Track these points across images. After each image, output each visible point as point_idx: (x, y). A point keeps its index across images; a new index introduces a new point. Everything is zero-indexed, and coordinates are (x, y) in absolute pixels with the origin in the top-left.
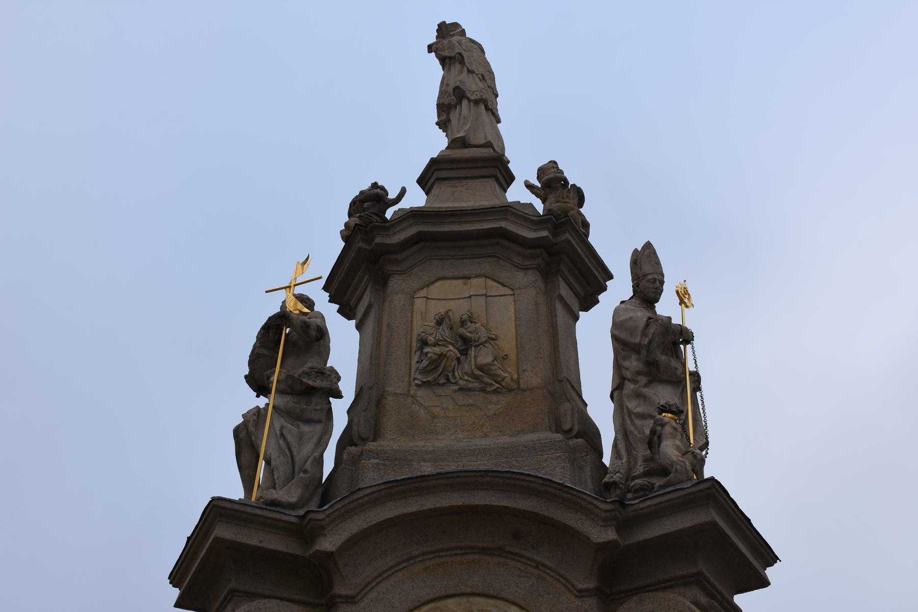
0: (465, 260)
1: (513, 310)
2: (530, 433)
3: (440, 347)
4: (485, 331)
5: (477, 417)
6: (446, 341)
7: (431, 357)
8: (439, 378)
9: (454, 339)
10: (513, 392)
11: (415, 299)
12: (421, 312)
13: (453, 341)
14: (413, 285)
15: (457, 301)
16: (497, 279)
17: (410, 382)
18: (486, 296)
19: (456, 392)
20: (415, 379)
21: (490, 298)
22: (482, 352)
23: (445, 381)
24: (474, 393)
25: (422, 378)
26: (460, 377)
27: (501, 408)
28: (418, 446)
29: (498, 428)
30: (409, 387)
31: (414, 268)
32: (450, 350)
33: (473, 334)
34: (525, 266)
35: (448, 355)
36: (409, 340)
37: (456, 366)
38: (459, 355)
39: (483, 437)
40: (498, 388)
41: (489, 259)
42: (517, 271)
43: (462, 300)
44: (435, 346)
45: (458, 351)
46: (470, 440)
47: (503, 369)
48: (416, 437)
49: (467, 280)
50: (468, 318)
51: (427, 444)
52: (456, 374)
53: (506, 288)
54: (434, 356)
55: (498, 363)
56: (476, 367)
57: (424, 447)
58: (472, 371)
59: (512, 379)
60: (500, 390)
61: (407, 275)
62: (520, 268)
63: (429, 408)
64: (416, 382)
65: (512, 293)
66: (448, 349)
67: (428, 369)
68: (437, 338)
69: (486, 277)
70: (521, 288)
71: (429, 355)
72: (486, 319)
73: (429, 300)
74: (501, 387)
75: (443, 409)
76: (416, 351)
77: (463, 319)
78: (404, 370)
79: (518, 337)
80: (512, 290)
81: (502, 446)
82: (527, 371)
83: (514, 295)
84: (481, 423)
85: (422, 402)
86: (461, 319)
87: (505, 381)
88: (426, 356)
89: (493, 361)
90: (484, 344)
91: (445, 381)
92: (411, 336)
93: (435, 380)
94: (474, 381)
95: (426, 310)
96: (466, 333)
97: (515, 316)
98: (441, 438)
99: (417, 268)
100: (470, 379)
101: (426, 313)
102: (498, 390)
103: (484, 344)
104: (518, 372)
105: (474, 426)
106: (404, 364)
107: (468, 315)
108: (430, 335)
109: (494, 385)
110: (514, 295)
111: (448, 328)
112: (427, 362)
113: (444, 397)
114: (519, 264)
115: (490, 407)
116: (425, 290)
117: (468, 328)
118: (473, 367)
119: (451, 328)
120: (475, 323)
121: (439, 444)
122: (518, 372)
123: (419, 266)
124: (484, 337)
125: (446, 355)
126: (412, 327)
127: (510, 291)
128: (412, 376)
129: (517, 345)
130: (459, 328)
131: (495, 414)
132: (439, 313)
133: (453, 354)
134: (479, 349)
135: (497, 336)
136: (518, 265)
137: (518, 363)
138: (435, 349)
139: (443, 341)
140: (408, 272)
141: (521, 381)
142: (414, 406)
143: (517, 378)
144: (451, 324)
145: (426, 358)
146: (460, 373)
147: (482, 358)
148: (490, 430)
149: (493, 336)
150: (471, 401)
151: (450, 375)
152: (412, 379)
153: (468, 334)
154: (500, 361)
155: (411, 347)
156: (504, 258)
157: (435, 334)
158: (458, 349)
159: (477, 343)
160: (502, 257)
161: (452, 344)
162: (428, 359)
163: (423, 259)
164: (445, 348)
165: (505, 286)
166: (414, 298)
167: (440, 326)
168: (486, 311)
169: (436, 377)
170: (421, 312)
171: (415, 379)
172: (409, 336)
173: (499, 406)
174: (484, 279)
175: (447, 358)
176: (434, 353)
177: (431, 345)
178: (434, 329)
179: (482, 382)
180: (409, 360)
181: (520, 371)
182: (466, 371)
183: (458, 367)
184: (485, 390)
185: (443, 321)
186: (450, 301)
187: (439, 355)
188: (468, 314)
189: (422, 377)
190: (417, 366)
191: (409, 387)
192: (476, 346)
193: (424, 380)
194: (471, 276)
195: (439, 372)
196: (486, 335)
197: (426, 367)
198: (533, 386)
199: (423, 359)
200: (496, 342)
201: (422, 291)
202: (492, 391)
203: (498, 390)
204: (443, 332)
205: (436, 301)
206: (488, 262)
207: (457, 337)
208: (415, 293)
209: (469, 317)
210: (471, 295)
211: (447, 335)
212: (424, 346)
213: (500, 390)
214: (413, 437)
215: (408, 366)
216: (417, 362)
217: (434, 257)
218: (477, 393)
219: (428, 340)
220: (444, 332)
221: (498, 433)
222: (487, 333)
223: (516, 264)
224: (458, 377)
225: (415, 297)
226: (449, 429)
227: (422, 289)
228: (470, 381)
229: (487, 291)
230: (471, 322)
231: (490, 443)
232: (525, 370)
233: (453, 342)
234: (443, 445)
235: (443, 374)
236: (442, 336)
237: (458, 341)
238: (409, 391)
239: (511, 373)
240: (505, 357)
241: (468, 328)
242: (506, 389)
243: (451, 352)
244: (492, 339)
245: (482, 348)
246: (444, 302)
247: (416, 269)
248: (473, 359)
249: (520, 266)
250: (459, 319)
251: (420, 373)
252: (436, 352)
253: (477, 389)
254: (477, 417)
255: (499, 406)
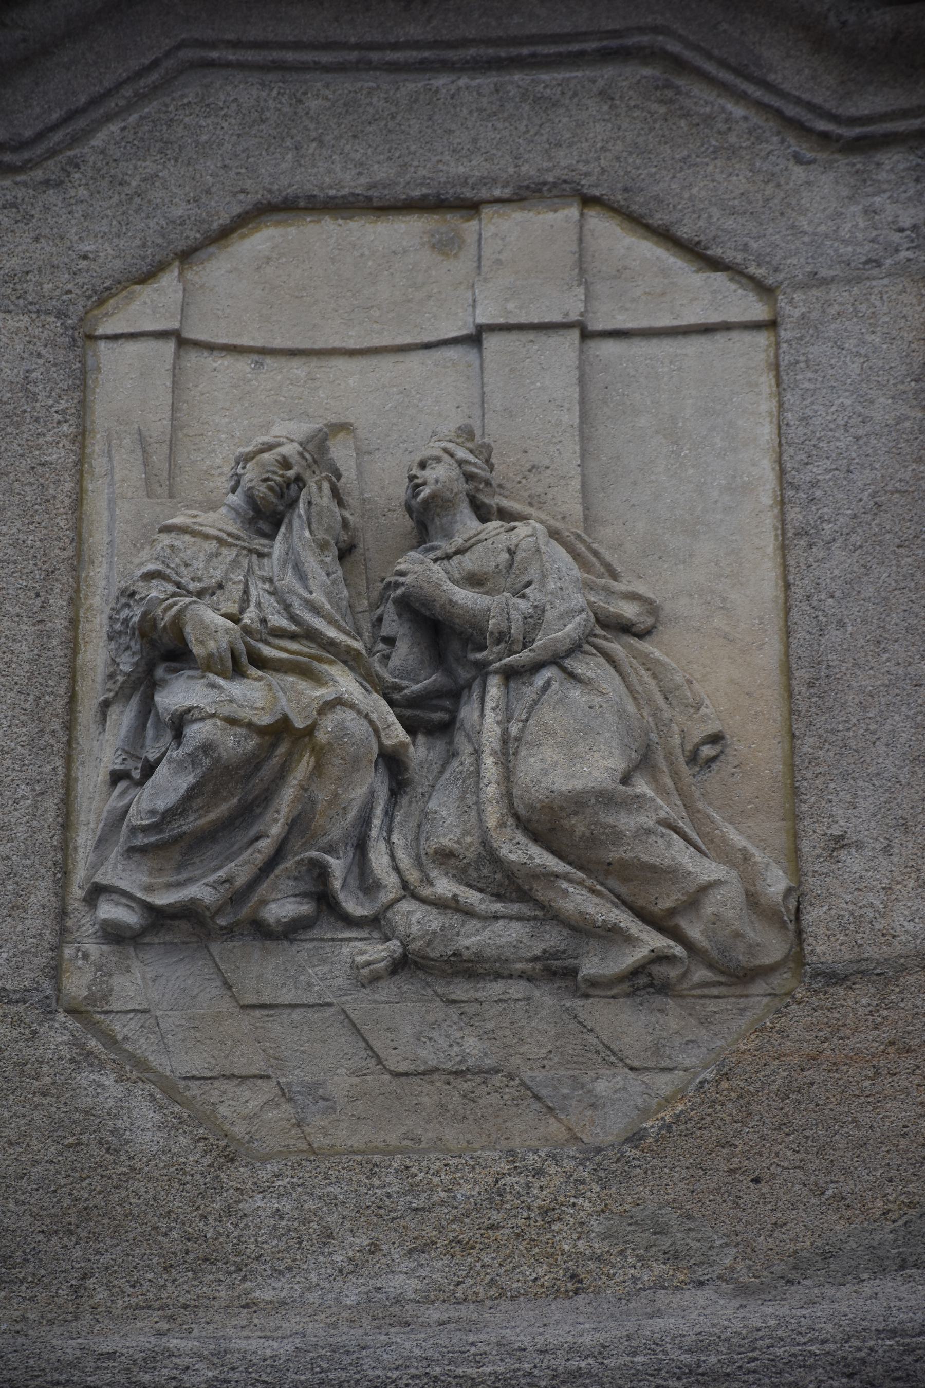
0: (441, 81)
1: (766, 432)
2: (880, 1270)
3: (273, 678)
4: (576, 572)
5: (512, 1154)
6: (310, 635)
7: (207, 748)
8: (263, 889)
9: (366, 626)
10: (760, 987)
11: (102, 345)
12: (142, 440)
13: (358, 633)
14: (86, 247)
15: (386, 366)
16: (658, 219)
17: (63, 913)
18: (586, 335)
19: (375, 979)
20: (97, 892)
21: (608, 349)
22: (548, 714)
23: (306, 908)
24: (497, 987)
25: (149, 889)
26: (405, 885)
27: (680, 1094)
28: (111, 1355)
29: (661, 1231)
30: (57, 948)
31: (88, 132)
32: (339, 702)
33: (500, 592)
34: (853, 121)
35: (321, 737)
36: (59, 624)
37: (379, 811)
38: (397, 734)
39: (556, 1292)
40: (660, 958)
41: (608, 72)
42: (798, 159)
43: (414, 361)
44: (237, 672)
45: (392, 703)
46: (466, 1311)
47: (694, 836)
48: (101, 1295)
49: (453, 219)
50: (461, 486)
51: (174, 1343)
52: (379, 860)
53: (719, 279)
54: (230, 741)
55: (661, 790)
56: (516, 816)
57: (151, 1360)
58: (485, 843)
59: (753, 900)
60: (673, 973)
61: (38, 174)
62: (825, 136)
63: (195, 1089)
64: (108, 910)
65: (758, 311)
66: (325, 693)
67: (191, 823)
68: (251, 615)
69: (588, 201)
70: (826, 282)
71: (196, 732)
72: (584, 485)
73: (193, 358)
74: (679, 950)
75: (286, 1094)
76: (105, 705)
77: (425, 492)
78: (21, 831)
79: (795, 614)
80: (765, 290)
81: (686, 1358)
82: (859, 846)
83: (772, 325)
84: (539, 1198)
85: (145, 1047)
86: (416, 488)
87: (708, 909)
88: (178, 736)
89: (626, 780)
90: (568, 663)
91: (306, 908)
92: (74, 602)
93: (238, 898)
94: (498, 907)
95: (175, 428)
96: (449, 586)
97: (782, 472)
98: (268, 1295)
99: (114, 127)
100: (472, 897)
101: (172, 445)
102: (656, 969)
103: (568, 663)
104: (795, 855)
105: (496, 1217)
106: (24, 789)
107: (461, 463)
108: (200, 594)
109: (629, 940)
110: (772, 325)
111: (323, 546)
112: (186, 781)
113: (296, 1015)
114: (810, 107)
115: (601, 1087)
116: (169, 280)
117: (460, 552)
118: (491, 821)
119: (345, 553)
120: (505, 515)
121: (254, 1344)
122: (795, 855)
123: (130, 107)
124: (571, 613)
125: (310, 731)
126: (78, 539)
127: (752, 297)
128: (80, 874)
129: (788, 672)
130: (403, 552)
131: (636, 1138)
132: (269, 447)
133: (358, 727)
134: (529, 692)
135: (652, 608)
136: (805, 116)
137: (795, 792)
138: (236, 689)
139: (293, 637)
140: (53, 153)
141: (811, 915)
142: (85, 1078)
143: (789, 891)
144: (345, 524)
145: (176, 754)
146: (400, 854)
147: (549, 753)
148: (599, 1247)
149: (629, 611)
150: (472, 1045)
151: (337, 865)
152: (77, 892)
153: (464, 596)
154: (675, 775)
155: (73, 674)
156: (710, 68)
157: (236, 591)
158: (389, 694)
159: (524, 656)
160: (699, 61)
161: (350, 659)
162: (193, 759)
163: (155, 64)
164: (303, 685)
165: (715, 264)
166: (91, 338)
167: (272, 537)
168: (584, 438)
169: (241, 881)
170: (142, 440)
171: (97, 892)
172: (58, 603)
173: (664, 1083)
174: (573, 212)
175: (320, 752)
176: (232, 721)
177: (209, 665)
178: (229, 554)
179: (552, 916)
180: (59, 762)
181: (805, 846)
182: (448, 841)
183: (389, 814)
184: (571, 973)
185: (292, 504)
186: (341, 364)
187: (262, 731)
188: (461, 454)
189: (146, 879)
190: (115, 802)
191: (57, 948)
192: (510, 675)
193: (161, 899)
194: (484, 194)
195: (266, 845)
196: (578, 600)
197: (169, 815)
198: (899, 949)
199: (152, 756)
200: (644, 646)
201: (146, 293)
202: (620, 979)
203: (656, 969)
204: (290, 578)
205: (243, 365)
206: (605, 95)
207: (389, 611)
208: (101, 302)
209: (469, 477)
210: (482, 330)
211: (318, 597)
212: (160, 672)
213: (673, 973)
214: (75, 1289)
215: (51, 803)
216: (116, 777)
217: (231, 56)
218: (517, 989)
219: (190, 632)
220: (302, 577)
221: (659, 1268)
222: (589, 586)
223: (791, 111)
224: (391, 880)
225: (100, 331)
226: (328, 1235)
227: (145, 279)
228: (468, 913)
229: (587, 299)
230: (482, 513)
231: (601, 1337)
232: (840, 842)
233: (357, 645)
234: (288, 1347)
235: (289, 863)
236: (287, 607)
237: (390, 641)
238: (55, 971)
239: (746, 857)
240: (707, 751)
241: (460, 552)
242: (711, 966)
243: (349, 715)
244: (625, 628)
245: (555, 686)
246: (298, 369)
247: (98, 140)
248: (488, 760)
249: (822, 125)
250: (401, 491)
251: (131, 851)
252: (245, 714)
253: (302, 204)
254: (512, 1154)
255: (664, 1083)
